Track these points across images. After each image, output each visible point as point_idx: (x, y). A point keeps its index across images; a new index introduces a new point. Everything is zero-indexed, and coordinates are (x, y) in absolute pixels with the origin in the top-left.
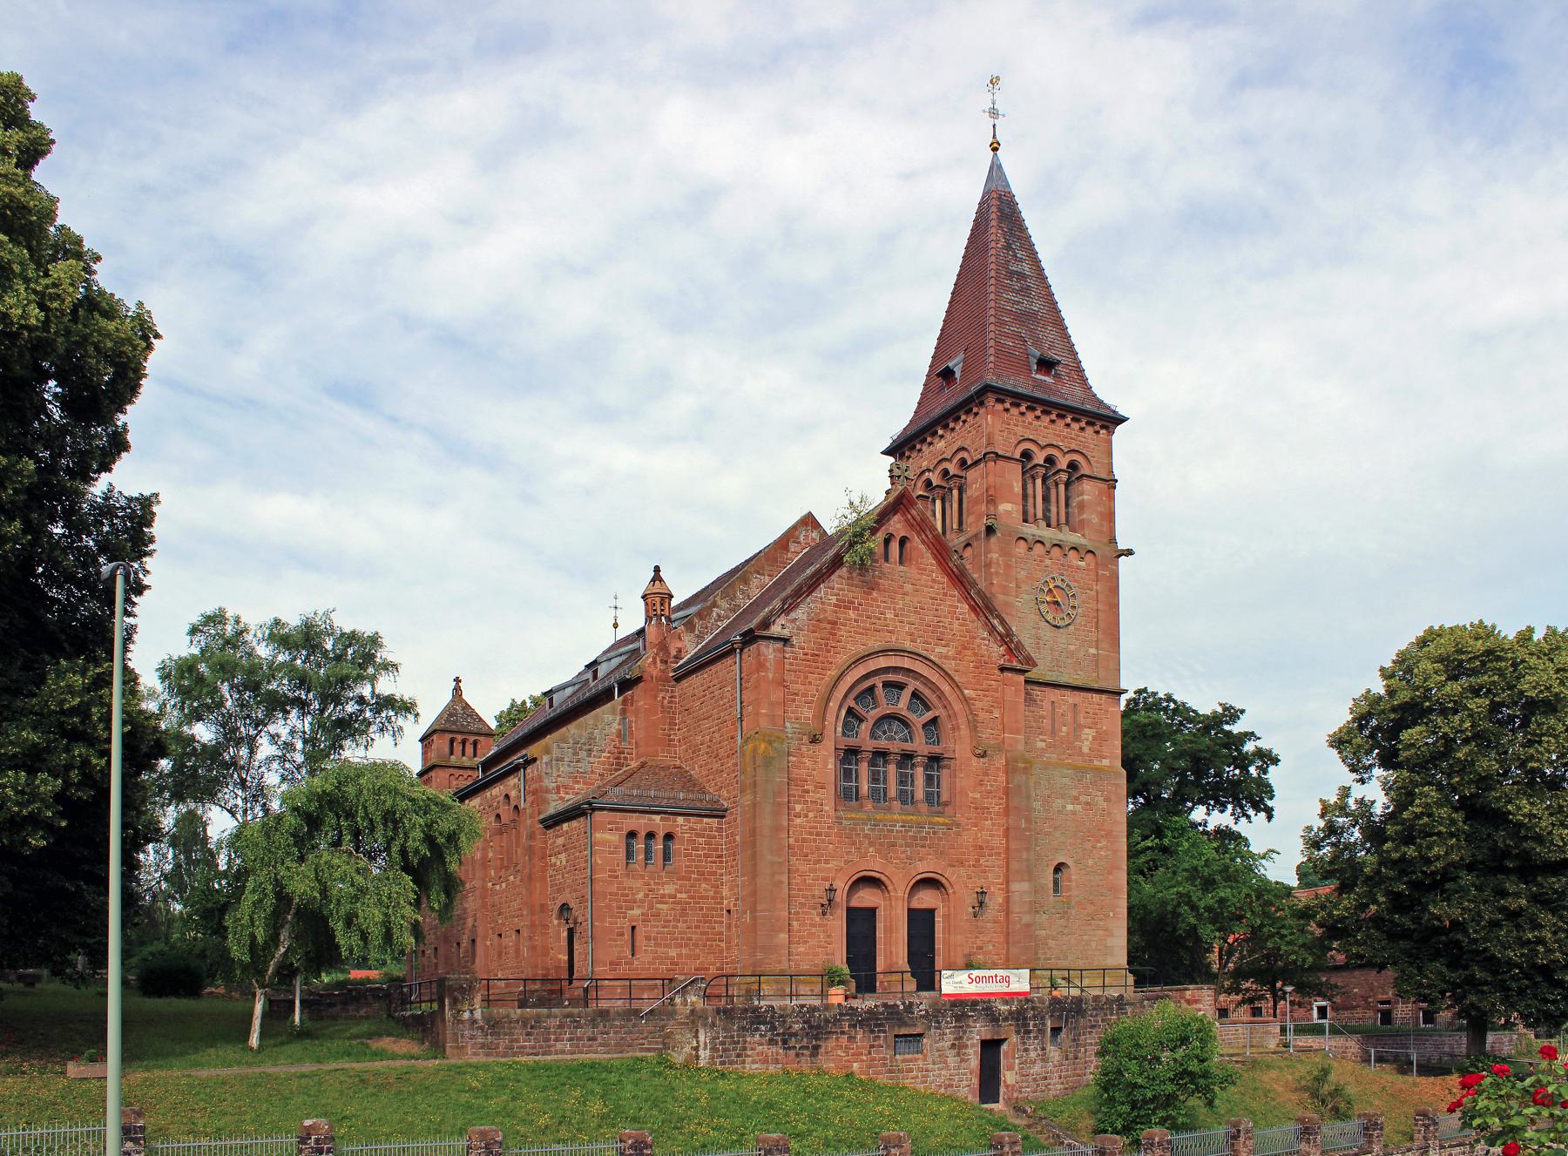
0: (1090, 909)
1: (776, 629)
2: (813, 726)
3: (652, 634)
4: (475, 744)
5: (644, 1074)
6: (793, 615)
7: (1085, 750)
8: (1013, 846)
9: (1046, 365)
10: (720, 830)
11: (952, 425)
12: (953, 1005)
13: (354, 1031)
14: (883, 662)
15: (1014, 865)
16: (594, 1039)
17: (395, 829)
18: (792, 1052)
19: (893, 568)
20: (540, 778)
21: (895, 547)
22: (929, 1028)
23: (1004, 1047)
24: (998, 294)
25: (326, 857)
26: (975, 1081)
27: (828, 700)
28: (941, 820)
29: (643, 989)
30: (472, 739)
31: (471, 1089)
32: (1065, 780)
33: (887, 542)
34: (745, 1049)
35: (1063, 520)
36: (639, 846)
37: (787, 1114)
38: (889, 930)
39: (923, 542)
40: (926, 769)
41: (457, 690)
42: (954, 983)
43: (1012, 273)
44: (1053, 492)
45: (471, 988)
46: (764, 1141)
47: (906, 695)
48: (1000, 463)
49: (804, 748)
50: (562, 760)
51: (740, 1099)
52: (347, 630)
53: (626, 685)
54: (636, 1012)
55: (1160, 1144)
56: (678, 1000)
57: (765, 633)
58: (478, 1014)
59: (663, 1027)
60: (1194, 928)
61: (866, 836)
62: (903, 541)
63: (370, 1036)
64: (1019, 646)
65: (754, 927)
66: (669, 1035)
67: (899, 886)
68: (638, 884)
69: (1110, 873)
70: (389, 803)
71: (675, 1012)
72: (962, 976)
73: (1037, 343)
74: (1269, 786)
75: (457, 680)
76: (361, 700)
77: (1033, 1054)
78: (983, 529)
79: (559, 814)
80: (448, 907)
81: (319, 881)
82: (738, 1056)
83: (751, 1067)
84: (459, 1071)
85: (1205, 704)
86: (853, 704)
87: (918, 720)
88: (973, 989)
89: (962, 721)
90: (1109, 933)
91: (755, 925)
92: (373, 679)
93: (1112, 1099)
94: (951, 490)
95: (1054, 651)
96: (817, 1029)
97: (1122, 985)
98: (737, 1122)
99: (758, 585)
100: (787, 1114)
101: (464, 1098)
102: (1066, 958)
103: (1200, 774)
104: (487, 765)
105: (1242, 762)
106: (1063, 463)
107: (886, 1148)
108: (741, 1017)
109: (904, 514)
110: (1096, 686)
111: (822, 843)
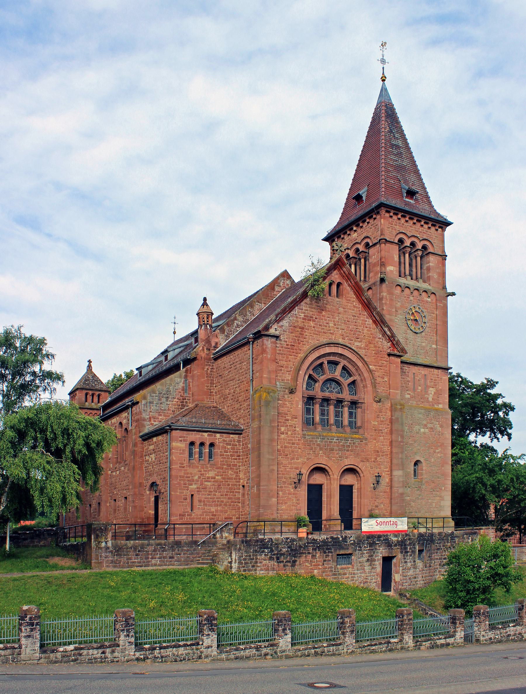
0: (433, 485)
1: (272, 331)
2: (291, 384)
3: (202, 335)
4: (99, 396)
5: (203, 577)
6: (281, 324)
7: (430, 399)
8: (394, 450)
9: (411, 194)
10: (239, 441)
11: (361, 225)
12: (368, 537)
13: (38, 553)
14: (328, 350)
15: (395, 461)
16: (173, 558)
17: (68, 439)
18: (282, 564)
19: (333, 300)
20: (140, 413)
21: (334, 287)
22: (355, 550)
23: (394, 561)
24: (386, 156)
25: (29, 455)
26: (379, 579)
27: (299, 370)
28: (357, 436)
29: (197, 529)
30: (97, 393)
31: (110, 587)
32: (420, 416)
33: (330, 285)
34: (256, 562)
35: (419, 276)
36: (196, 450)
37: (284, 599)
38: (329, 496)
39: (349, 285)
40: (349, 409)
41: (89, 367)
42: (369, 525)
43: (392, 146)
44: (414, 261)
45: (106, 529)
46: (278, 615)
47: (339, 368)
48: (388, 245)
49: (286, 396)
50: (152, 403)
51: (257, 591)
52: (28, 335)
53: (187, 362)
54: (196, 542)
55: (483, 614)
56: (218, 535)
57: (266, 333)
58: (110, 544)
59: (210, 550)
60: (484, 496)
61: (318, 445)
62: (339, 285)
63: (48, 556)
64: (398, 342)
65: (258, 496)
66: (216, 555)
67: (335, 471)
68: (195, 471)
69: (443, 466)
70: (66, 424)
71: (216, 542)
72: (373, 521)
73: (406, 182)
74: (510, 422)
75: (90, 361)
76: (34, 374)
77: (409, 565)
78: (379, 279)
79: (152, 432)
80: (96, 482)
81: (26, 468)
82: (253, 566)
83: (260, 573)
84: (102, 576)
85: (477, 380)
86: (311, 372)
87: (345, 382)
88: (378, 528)
89: (368, 383)
90: (442, 498)
91: (259, 494)
92: (41, 363)
93: (455, 589)
94: (360, 259)
95: (416, 346)
96: (295, 551)
97: (450, 527)
98: (257, 604)
99: (259, 308)
100: (284, 599)
101: (106, 592)
102: (420, 512)
103: (474, 415)
104: (105, 407)
105: (495, 409)
106: (419, 246)
107: (342, 618)
108: (253, 544)
109: (339, 270)
110: (436, 365)
111: (294, 450)
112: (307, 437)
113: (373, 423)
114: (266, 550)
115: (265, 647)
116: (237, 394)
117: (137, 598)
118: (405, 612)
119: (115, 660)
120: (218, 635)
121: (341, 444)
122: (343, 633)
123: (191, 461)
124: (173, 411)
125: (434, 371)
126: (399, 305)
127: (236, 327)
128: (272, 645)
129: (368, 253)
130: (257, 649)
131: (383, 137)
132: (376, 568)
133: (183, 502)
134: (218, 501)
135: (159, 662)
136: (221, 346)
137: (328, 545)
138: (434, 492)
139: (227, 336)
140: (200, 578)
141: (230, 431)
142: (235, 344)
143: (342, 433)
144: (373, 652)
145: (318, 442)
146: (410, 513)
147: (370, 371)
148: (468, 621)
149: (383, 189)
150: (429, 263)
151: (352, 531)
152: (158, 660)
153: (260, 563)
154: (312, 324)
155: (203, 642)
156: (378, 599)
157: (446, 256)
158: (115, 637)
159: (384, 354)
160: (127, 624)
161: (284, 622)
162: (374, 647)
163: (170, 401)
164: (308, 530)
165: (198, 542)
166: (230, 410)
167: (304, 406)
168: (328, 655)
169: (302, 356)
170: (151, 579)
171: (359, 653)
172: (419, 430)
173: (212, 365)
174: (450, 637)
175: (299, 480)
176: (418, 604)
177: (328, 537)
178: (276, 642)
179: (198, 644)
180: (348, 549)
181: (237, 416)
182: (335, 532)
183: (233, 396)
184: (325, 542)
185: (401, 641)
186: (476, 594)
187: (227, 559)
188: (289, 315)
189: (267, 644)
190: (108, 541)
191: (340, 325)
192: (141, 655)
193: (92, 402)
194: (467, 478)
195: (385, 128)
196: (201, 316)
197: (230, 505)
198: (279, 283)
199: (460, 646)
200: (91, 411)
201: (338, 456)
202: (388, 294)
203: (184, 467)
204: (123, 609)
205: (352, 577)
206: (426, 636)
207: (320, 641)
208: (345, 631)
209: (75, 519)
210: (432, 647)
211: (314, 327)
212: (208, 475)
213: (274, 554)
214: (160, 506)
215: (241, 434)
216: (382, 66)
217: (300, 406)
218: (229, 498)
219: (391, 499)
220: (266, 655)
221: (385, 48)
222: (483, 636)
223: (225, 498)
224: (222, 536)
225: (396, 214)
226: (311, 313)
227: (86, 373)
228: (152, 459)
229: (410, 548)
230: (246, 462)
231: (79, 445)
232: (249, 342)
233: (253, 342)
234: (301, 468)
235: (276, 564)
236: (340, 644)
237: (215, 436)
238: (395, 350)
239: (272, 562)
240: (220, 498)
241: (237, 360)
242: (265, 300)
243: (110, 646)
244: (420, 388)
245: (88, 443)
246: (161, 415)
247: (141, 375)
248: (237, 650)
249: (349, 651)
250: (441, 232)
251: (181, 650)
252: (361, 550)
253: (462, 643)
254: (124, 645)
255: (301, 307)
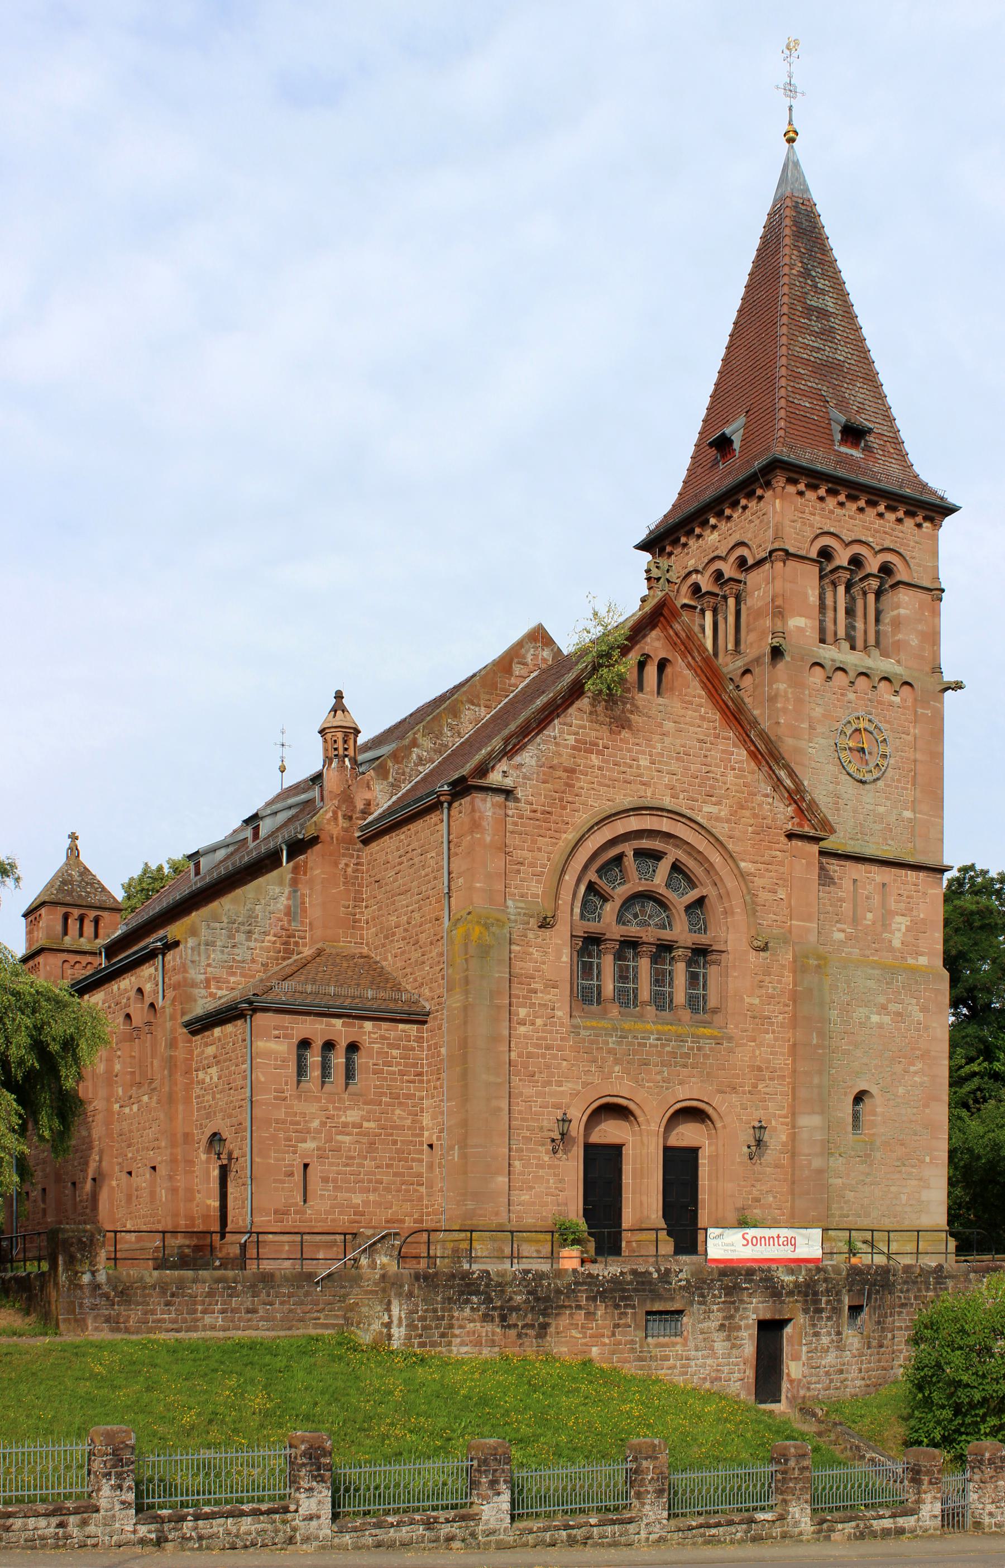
1: (495, 778)
3: (332, 780)
4: (96, 921)
7: (897, 943)
9: (854, 434)
10: (420, 1039)
12: (723, 1273)
14: (634, 824)
16: (254, 1311)
18: (513, 1332)
20: (184, 968)
21: (651, 671)
22: (691, 1303)
23: (788, 1330)
26: (750, 1373)
27: (563, 872)
28: (707, 1031)
29: (318, 1246)
30: (92, 914)
31: (93, 1376)
32: (871, 984)
33: (642, 665)
34: (451, 1326)
35: (872, 641)
36: (314, 1058)
39: (689, 666)
42: (724, 1245)
43: (809, 311)
44: (860, 603)
47: (664, 867)
49: (531, 935)
50: (213, 944)
53: (298, 847)
54: (309, 1276)
55: (991, 1461)
56: (364, 1261)
61: (610, 1051)
64: (813, 805)
68: (313, 1108)
71: (360, 1277)
73: (842, 404)
75: (73, 837)
77: (825, 1340)
79: (209, 1015)
84: (77, 1352)
87: (679, 900)
93: (927, 1403)
94: (725, 598)
95: (858, 814)
96: (543, 1303)
97: (939, 1252)
98: (442, 1422)
99: (471, 718)
101: (84, 1388)
104: (112, 949)
106: (873, 565)
107: (635, 1459)
108: (448, 1286)
110: (911, 859)
112: (583, 1032)
113: (747, 1000)
114: (475, 1299)
115: (447, 1521)
116: (415, 926)
117: (154, 1402)
118: (792, 1450)
119: (89, 1542)
120: (335, 1491)
121: (668, 1049)
122: (639, 1495)
123: (302, 1085)
124: (265, 965)
125: (906, 876)
126: (818, 712)
127: (416, 765)
128: (463, 1518)
129: (745, 583)
130: (429, 1524)
131: (786, 289)
132: (741, 1345)
133: (283, 1182)
134: (370, 1181)
135: (192, 1549)
136: (380, 811)
137: (624, 1290)
138: (904, 1169)
139: (393, 785)
140: (313, 1360)
141: (398, 1016)
142: (421, 799)
143: (671, 1025)
144: (712, 1541)
145: (611, 1045)
146: (842, 1216)
147: (742, 875)
148: (952, 1480)
149: (782, 424)
150: (898, 607)
151: (694, 1258)
152: (191, 1544)
153: (461, 1327)
154: (595, 760)
155: (298, 1506)
156: (739, 1418)
157: (943, 591)
158: (90, 1489)
159: (778, 835)
160: (119, 1462)
161: (493, 1466)
162: (713, 1531)
163: (256, 940)
164: (587, 1252)
165: (316, 1275)
166: (399, 964)
167: (575, 959)
168: (602, 1545)
169: (570, 837)
170: (194, 1360)
171: (679, 1544)
172: (868, 1018)
173: (358, 857)
174: (905, 1514)
175: (563, 1134)
176: (843, 1433)
177: (625, 1270)
178: (475, 1509)
179: (286, 1510)
180: (672, 1299)
181: (415, 980)
182: (641, 1259)
183: (406, 930)
184: (616, 1283)
185: (782, 1518)
186: (976, 1415)
187: (379, 1318)
188: (538, 739)
189: (451, 1514)
190: (98, 1270)
191: (667, 764)
192: (150, 1532)
193: (81, 935)
194: (991, 1135)
195: (791, 267)
196: (329, 736)
197: (399, 1191)
198: (524, 657)
199: (932, 1536)
200: (78, 958)
201: (659, 1077)
202: (790, 686)
203: (285, 1099)
204: (109, 1427)
205: (683, 1366)
206: (845, 1508)
207: (582, 1511)
208: (642, 1489)
209: (40, 1215)
210: (861, 1536)
211: (600, 768)
212: (343, 1119)
213: (494, 1308)
214: (230, 1190)
215: (425, 1022)
216: (787, 101)
217: (565, 958)
218: (395, 1174)
219: (793, 1182)
220: (450, 1539)
221: (795, 54)
222: (991, 1514)
223: (387, 1174)
224: (374, 1262)
225: (814, 487)
226: (593, 734)
227: (66, 864)
228: (211, 1078)
229: (828, 1302)
230: (435, 1088)
231: (19, 1047)
232: (442, 803)
233: (450, 804)
234: (568, 1107)
235: (498, 1330)
236: (630, 1521)
237: (361, 1027)
238: (806, 824)
239: (489, 1327)
240: (374, 1174)
241: (415, 845)
242: (487, 697)
243: (76, 1512)
244: (869, 916)
245: (42, 1042)
246: (234, 974)
247: (197, 873)
248: (379, 1525)
249: (652, 1537)
250: (930, 531)
251: (247, 1524)
252: (704, 1303)
253: (935, 1529)
254: (111, 1509)
255: (568, 720)
